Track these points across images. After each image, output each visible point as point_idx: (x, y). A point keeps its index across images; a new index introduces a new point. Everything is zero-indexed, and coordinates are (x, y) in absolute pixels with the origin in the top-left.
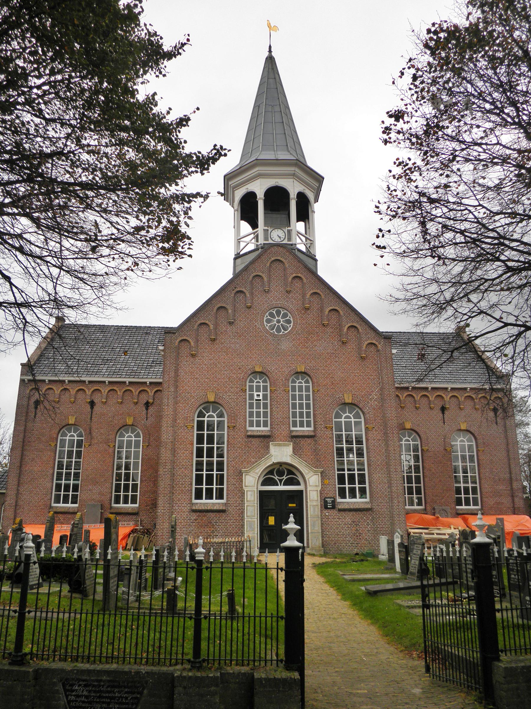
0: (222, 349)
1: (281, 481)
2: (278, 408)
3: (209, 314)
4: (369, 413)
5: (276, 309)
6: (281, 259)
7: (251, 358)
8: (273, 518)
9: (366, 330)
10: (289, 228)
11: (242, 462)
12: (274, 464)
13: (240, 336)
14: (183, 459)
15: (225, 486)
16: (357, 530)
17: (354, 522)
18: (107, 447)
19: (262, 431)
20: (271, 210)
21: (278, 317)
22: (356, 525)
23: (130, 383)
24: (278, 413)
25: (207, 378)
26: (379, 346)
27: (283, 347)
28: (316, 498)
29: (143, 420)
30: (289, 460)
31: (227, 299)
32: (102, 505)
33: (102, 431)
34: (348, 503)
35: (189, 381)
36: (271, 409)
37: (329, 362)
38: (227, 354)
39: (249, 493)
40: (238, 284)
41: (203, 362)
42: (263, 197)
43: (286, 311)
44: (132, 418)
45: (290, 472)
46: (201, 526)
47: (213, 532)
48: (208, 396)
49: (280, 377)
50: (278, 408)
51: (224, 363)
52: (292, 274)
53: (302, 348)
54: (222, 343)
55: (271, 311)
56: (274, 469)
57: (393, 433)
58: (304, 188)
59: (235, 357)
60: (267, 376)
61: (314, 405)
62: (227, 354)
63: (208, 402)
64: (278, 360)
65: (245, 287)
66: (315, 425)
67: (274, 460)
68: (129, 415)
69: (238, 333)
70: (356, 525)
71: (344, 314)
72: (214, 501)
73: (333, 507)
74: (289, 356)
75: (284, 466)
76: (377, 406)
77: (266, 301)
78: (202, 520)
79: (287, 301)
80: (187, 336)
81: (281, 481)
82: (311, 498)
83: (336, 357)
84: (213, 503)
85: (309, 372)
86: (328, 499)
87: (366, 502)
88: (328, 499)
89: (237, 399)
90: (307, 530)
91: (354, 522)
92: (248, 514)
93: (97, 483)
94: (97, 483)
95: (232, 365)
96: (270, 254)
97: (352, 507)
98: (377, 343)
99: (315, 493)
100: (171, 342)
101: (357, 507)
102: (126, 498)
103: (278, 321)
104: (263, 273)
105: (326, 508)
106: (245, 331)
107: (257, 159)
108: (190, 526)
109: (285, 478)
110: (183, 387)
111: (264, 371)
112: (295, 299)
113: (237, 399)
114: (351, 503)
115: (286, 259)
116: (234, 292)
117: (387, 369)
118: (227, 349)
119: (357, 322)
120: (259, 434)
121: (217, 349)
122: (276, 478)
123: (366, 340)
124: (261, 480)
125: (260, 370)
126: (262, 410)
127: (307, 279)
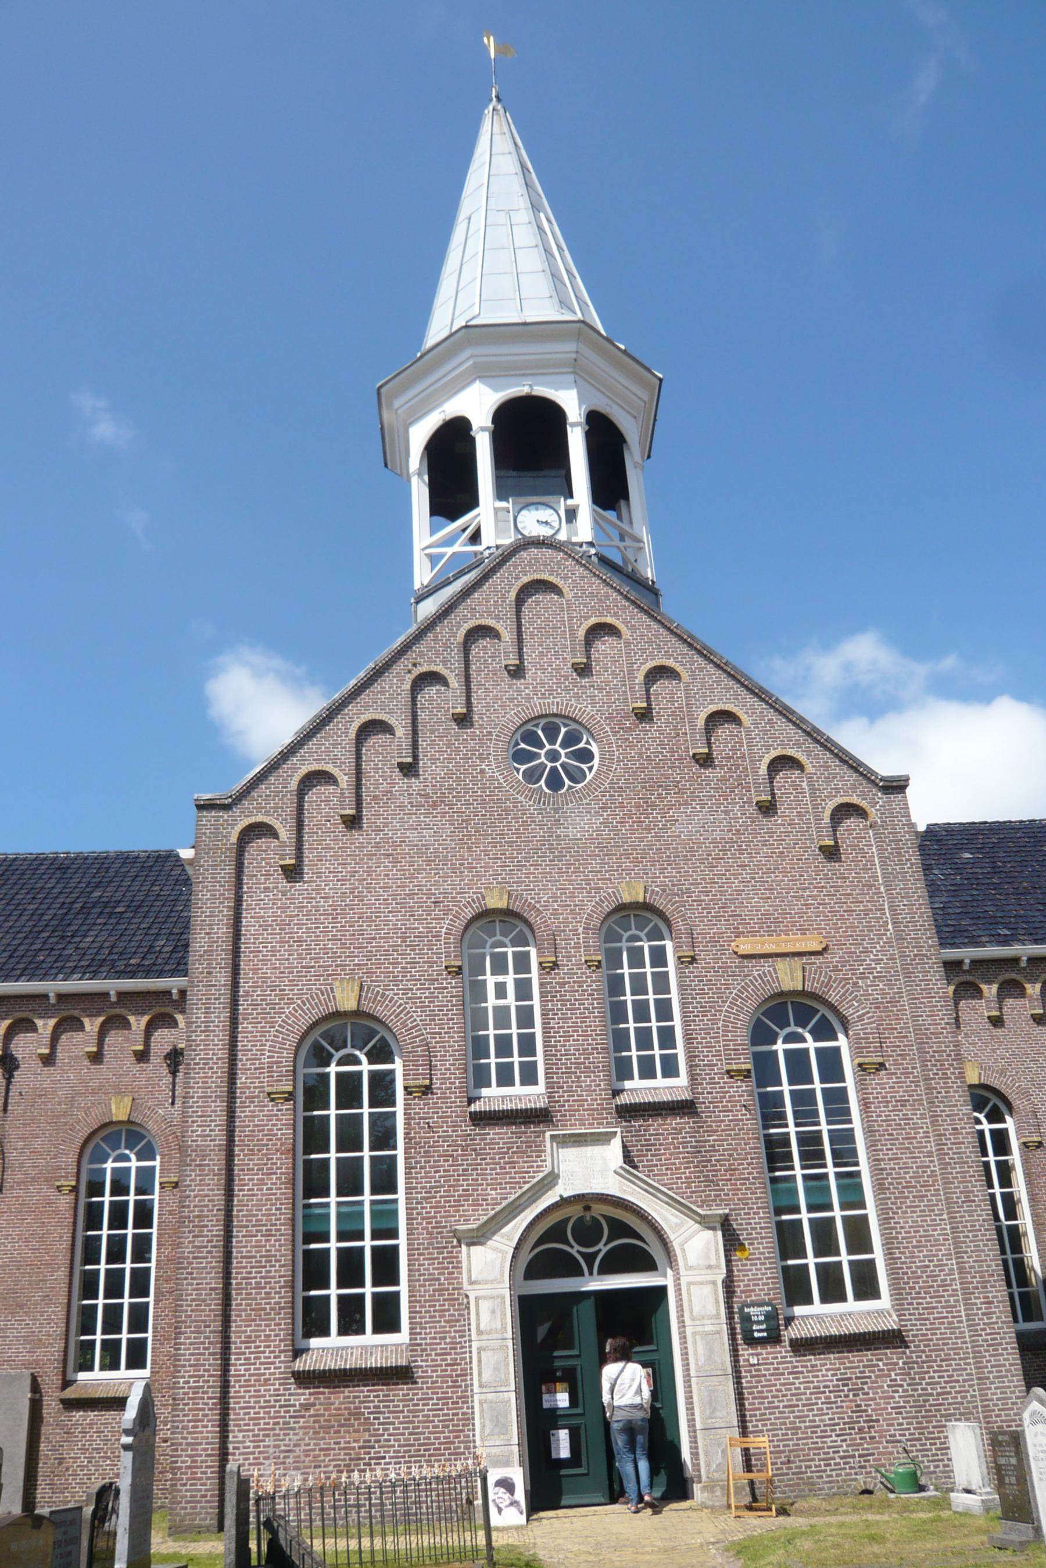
0: (377, 846)
1: (590, 1259)
2: (565, 1019)
3: (335, 745)
4: (861, 1018)
5: (543, 722)
6: (551, 579)
7: (470, 869)
8: (567, 1431)
9: (827, 767)
10: (569, 502)
11: (458, 1204)
12: (564, 1202)
13: (435, 805)
14: (259, 1206)
15: (403, 1288)
16: (858, 1409)
17: (845, 1381)
18: (52, 1193)
19: (520, 1098)
20: (516, 468)
21: (552, 742)
22: (856, 1391)
23: (121, 995)
24: (567, 1036)
25: (334, 939)
26: (872, 811)
27: (571, 832)
28: (711, 1309)
29: (160, 1104)
30: (613, 1186)
31: (391, 698)
32: (34, 1379)
33: (37, 1145)
34: (819, 1318)
35: (274, 951)
36: (545, 1024)
37: (720, 869)
38: (396, 861)
39: (484, 1306)
40: (421, 654)
41: (318, 890)
42: (488, 423)
43: (574, 726)
44: (128, 1101)
45: (620, 1229)
46: (327, 1428)
47: (367, 1446)
48: (338, 993)
49: (566, 922)
50: (565, 1019)
51: (386, 888)
52: (587, 618)
53: (633, 831)
54: (378, 830)
55: (529, 727)
56: (568, 1219)
57: (945, 1077)
58: (607, 401)
59: (418, 871)
60: (526, 921)
61: (684, 1005)
62: (396, 861)
63: (337, 1014)
64: (560, 871)
65: (444, 662)
66: (691, 1067)
67: (564, 1189)
68: (119, 1093)
69: (426, 795)
70: (856, 1391)
71: (756, 724)
72: (369, 1338)
73: (773, 1338)
74: (593, 855)
75: (599, 1210)
76: (884, 994)
77: (511, 700)
78: (327, 1407)
79: (577, 696)
80: (267, 813)
81: (590, 1259)
82: (697, 1309)
83: (741, 851)
84: (365, 1348)
85: (660, 903)
86: (752, 1311)
87: (880, 1313)
88: (752, 1311)
89: (432, 998)
90: (691, 1422)
91: (845, 1381)
92: (485, 1377)
93: (21, 1306)
94: (21, 1306)
95: (411, 895)
96: (515, 566)
97: (834, 1331)
98: (864, 804)
99: (707, 1290)
100: (216, 834)
101: (853, 1329)
102: (111, 1348)
103: (553, 756)
104: (497, 618)
105: (751, 1341)
106: (451, 789)
107: (466, 327)
108: (287, 1428)
109: (603, 1248)
110: (255, 971)
111: (516, 907)
112: (600, 690)
113: (432, 998)
114: (832, 1317)
115: (565, 578)
116: (412, 676)
117: (905, 880)
118: (395, 846)
119: (798, 745)
120: (508, 1106)
121: (361, 847)
122: (575, 1250)
123: (831, 797)
124: (526, 1257)
125: (502, 904)
126: (516, 1059)
127: (633, 628)
